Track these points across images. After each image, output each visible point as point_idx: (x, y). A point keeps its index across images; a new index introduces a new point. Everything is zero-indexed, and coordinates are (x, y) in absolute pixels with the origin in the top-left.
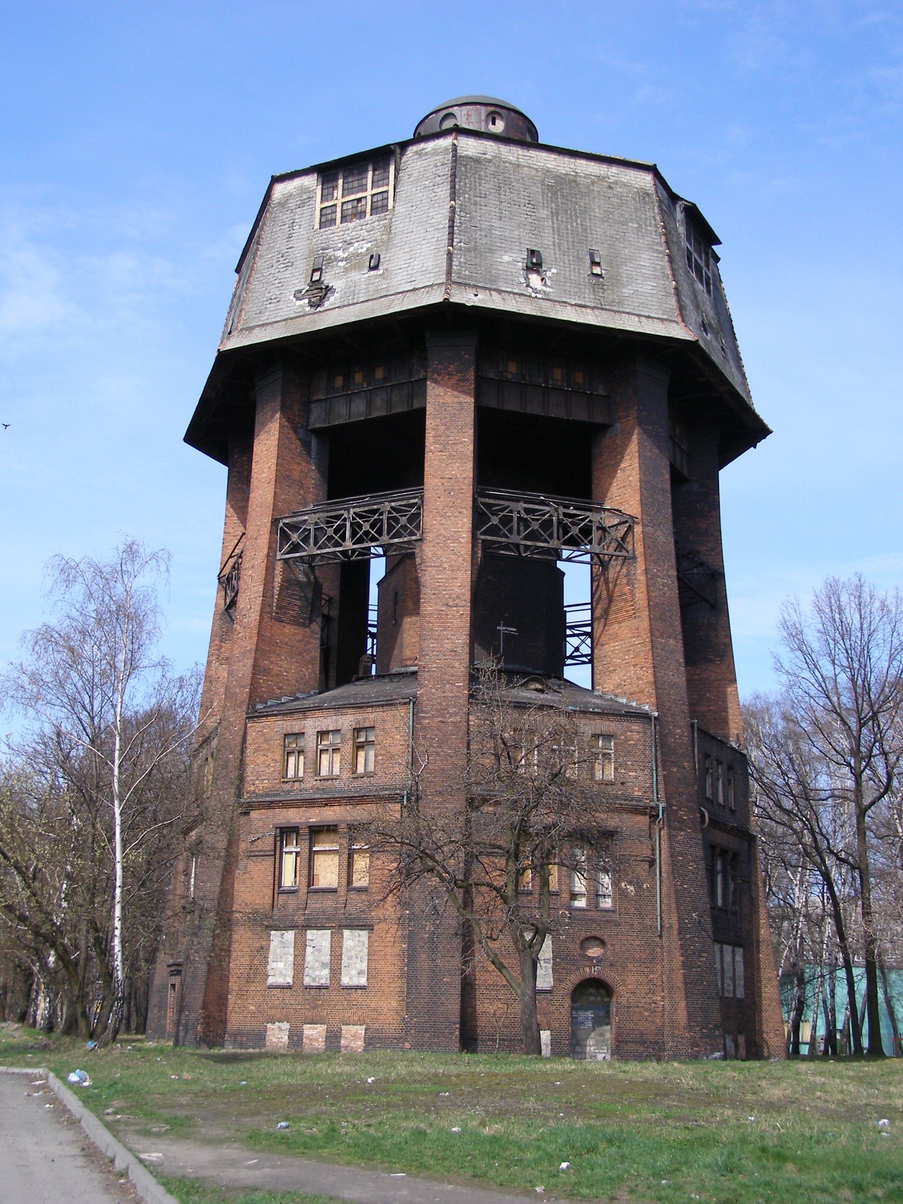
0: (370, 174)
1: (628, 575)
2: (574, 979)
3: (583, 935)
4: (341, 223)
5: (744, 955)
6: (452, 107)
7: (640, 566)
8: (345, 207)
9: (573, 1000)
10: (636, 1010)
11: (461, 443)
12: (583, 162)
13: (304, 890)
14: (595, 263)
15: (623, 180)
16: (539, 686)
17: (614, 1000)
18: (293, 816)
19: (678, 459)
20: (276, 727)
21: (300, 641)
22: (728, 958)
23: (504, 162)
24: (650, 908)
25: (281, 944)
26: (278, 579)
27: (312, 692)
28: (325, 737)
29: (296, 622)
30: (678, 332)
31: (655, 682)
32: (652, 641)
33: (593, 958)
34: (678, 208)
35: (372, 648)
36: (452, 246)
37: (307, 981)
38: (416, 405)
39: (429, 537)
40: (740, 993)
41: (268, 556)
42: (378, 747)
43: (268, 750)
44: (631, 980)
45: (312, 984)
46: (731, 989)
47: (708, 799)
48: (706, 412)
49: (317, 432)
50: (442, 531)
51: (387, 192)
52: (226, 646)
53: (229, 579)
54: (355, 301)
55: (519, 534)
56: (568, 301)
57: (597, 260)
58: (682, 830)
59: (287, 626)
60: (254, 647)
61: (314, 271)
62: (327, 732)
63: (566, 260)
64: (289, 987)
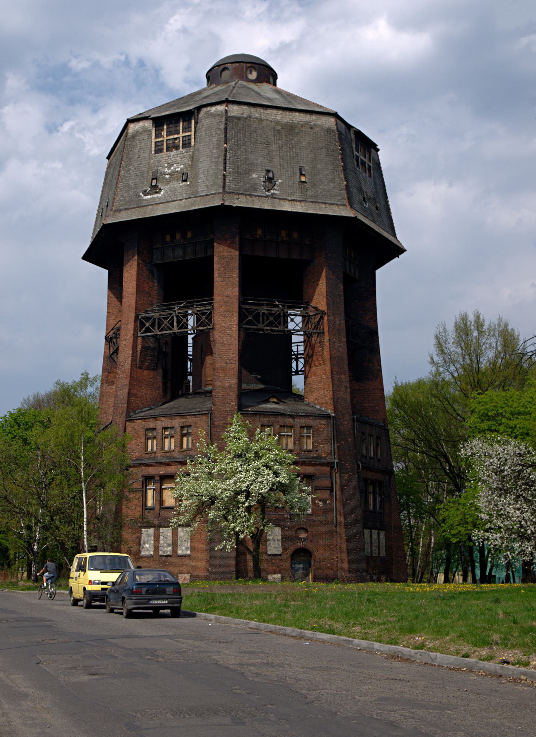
0: (181, 124)
1: (320, 342)
2: (292, 549)
3: (297, 527)
4: (167, 151)
5: (386, 535)
6: (227, 63)
7: (326, 338)
8: (168, 143)
9: (292, 559)
10: (324, 563)
11: (232, 277)
12: (297, 114)
13: (158, 508)
14: (301, 174)
15: (319, 123)
16: (275, 400)
17: (313, 558)
18: (151, 471)
19: (353, 270)
20: (140, 425)
21: (152, 378)
22: (375, 536)
23: (254, 118)
24: (330, 513)
25: (147, 533)
26: (139, 347)
27: (159, 405)
28: (166, 430)
29: (149, 368)
30: (346, 212)
31: (333, 398)
32: (332, 377)
33: (302, 538)
34: (352, 133)
35: (191, 368)
36: (225, 171)
37: (161, 553)
38: (209, 254)
39: (217, 327)
40: (383, 554)
41: (134, 334)
42: (193, 436)
43: (138, 437)
44: (321, 548)
45: (163, 554)
46: (377, 552)
47: (363, 456)
48: (368, 245)
49: (157, 266)
50: (223, 325)
51: (190, 135)
52: (111, 376)
53: (111, 339)
54: (175, 199)
55: (263, 323)
56: (287, 198)
57: (303, 173)
58: (346, 473)
59: (145, 371)
60: (128, 383)
61: (153, 179)
62: (168, 428)
63: (287, 175)
64: (151, 556)
